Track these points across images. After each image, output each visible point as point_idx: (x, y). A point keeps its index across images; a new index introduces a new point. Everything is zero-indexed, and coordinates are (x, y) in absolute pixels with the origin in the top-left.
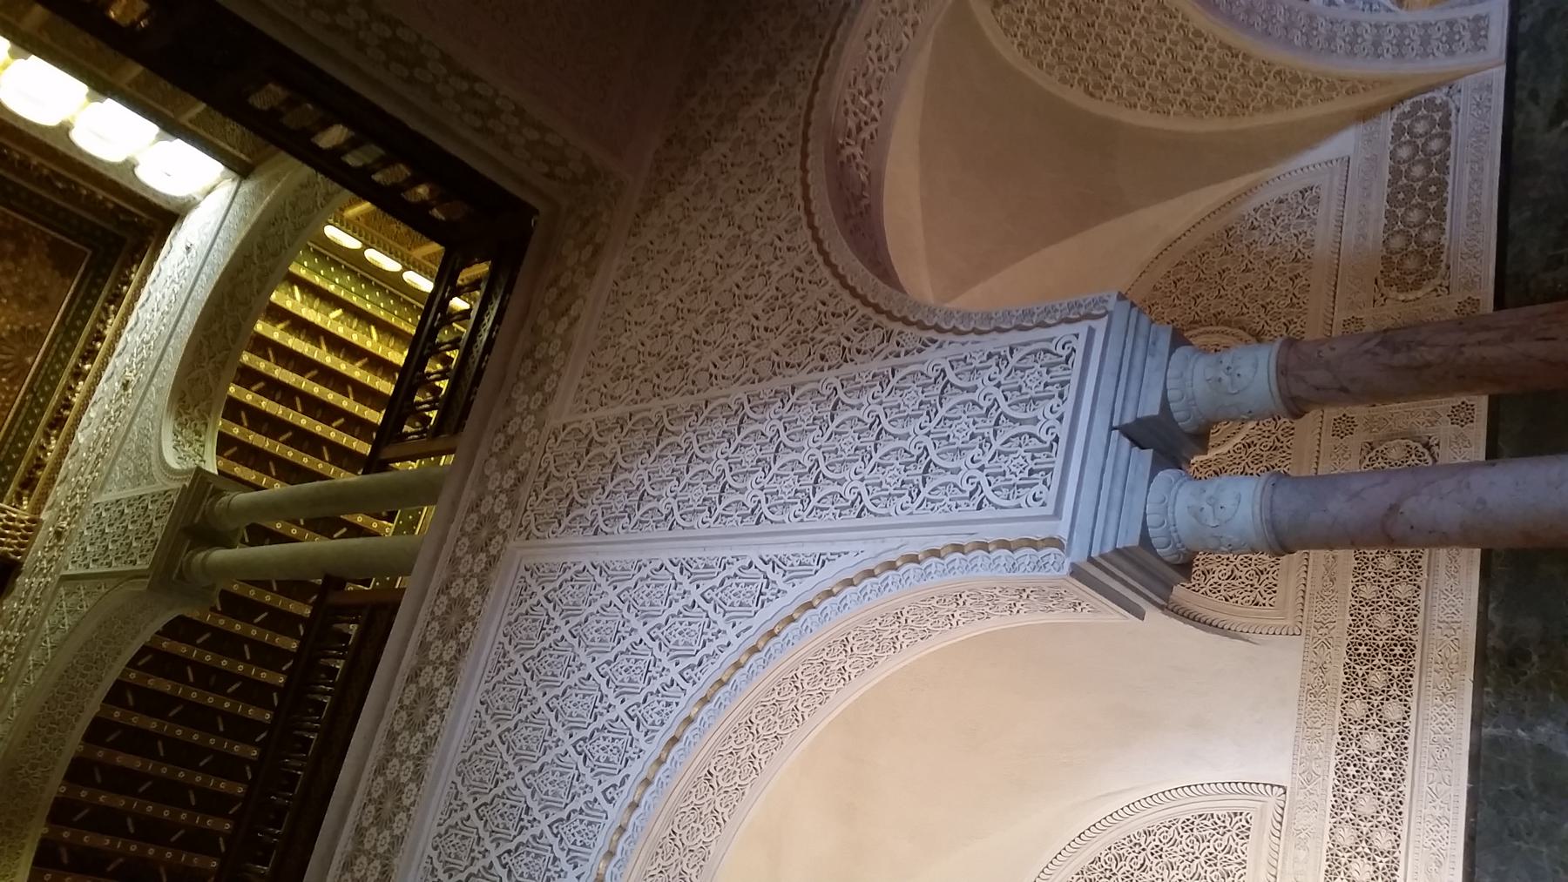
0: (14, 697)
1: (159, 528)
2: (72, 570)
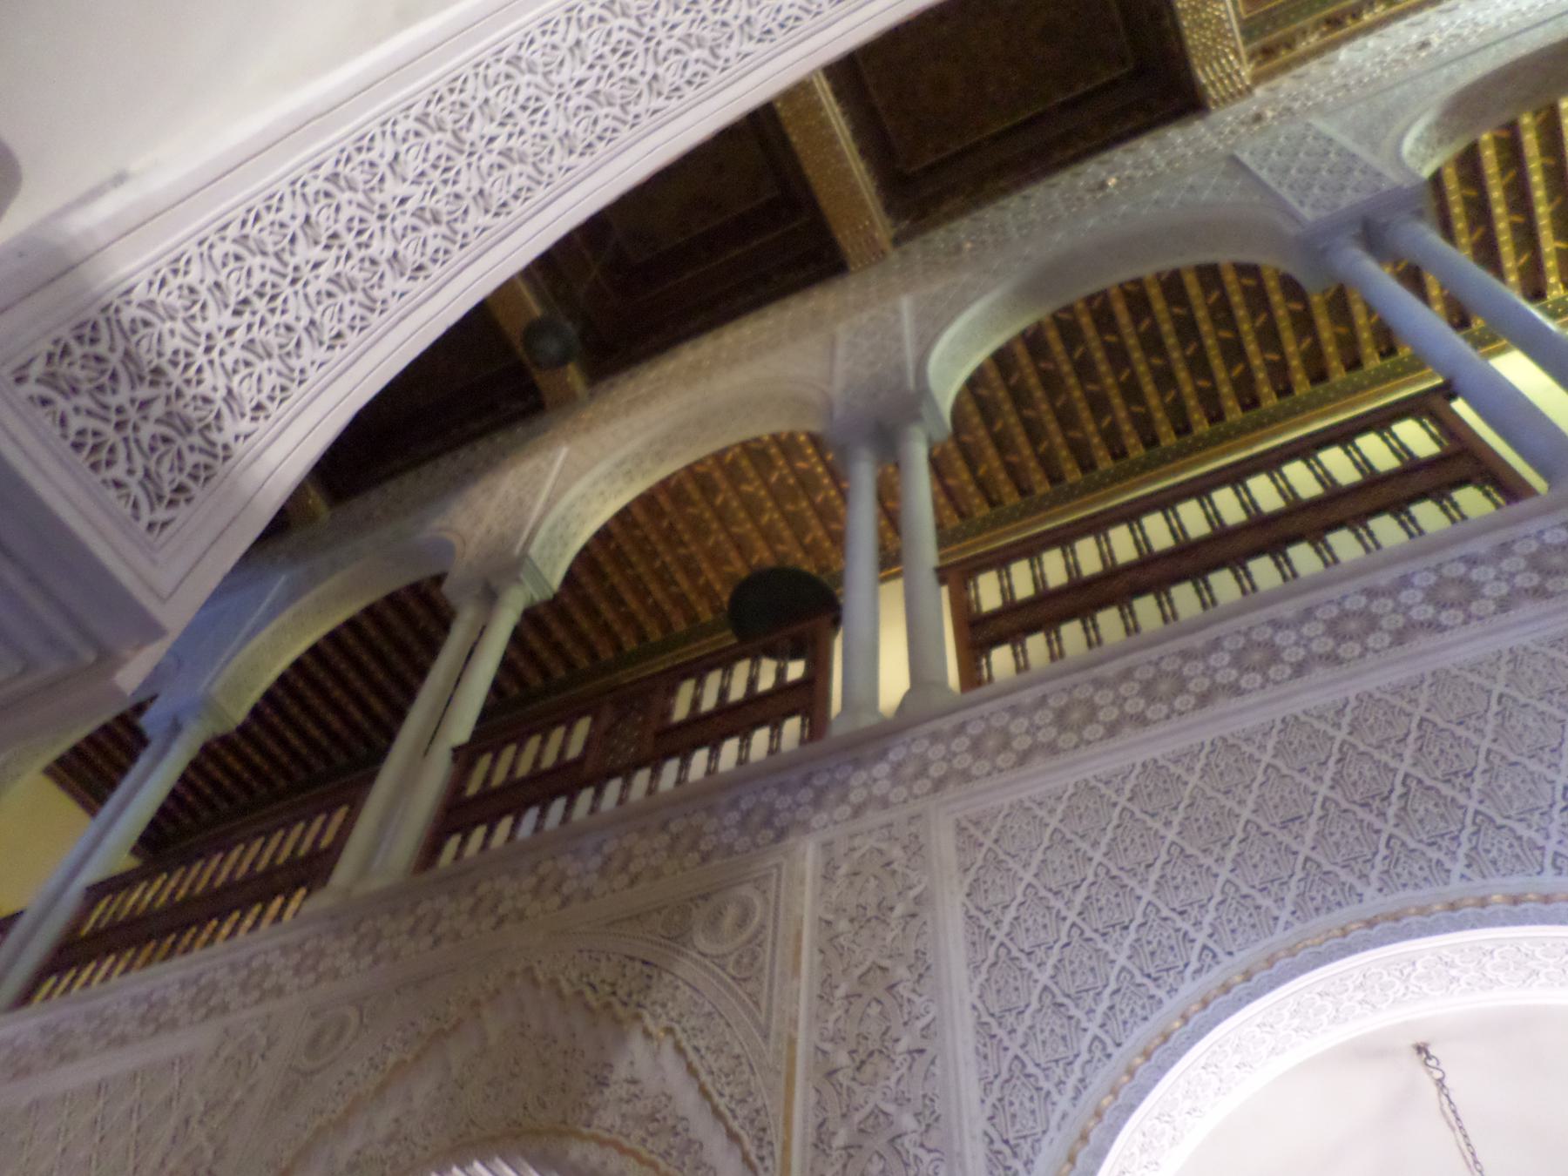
0: (1124, 207)
1: (1349, 198)
2: (1245, 157)
